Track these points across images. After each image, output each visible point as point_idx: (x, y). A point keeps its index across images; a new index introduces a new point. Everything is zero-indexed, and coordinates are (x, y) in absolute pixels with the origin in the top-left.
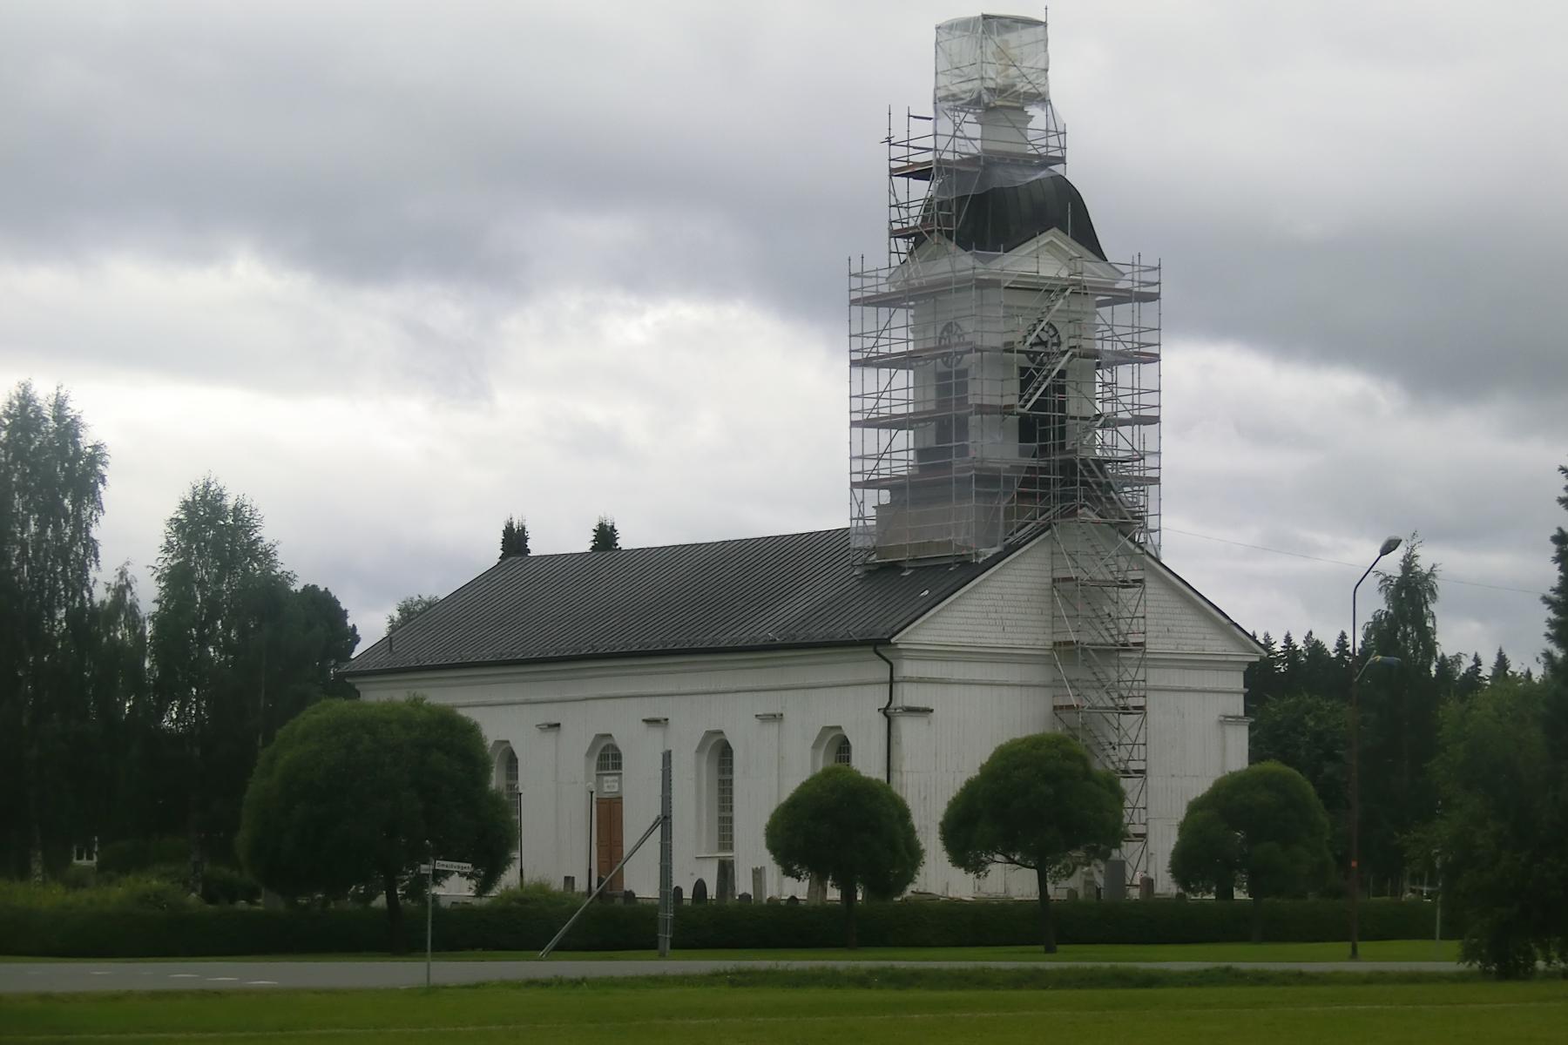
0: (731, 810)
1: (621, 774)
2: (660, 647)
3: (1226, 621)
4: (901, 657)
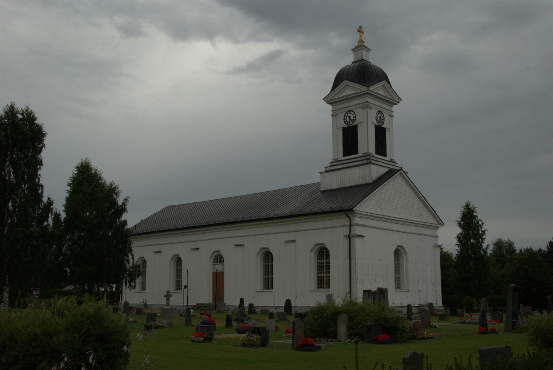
1: (224, 264)
2: (243, 220)
3: (434, 213)
4: (355, 216)
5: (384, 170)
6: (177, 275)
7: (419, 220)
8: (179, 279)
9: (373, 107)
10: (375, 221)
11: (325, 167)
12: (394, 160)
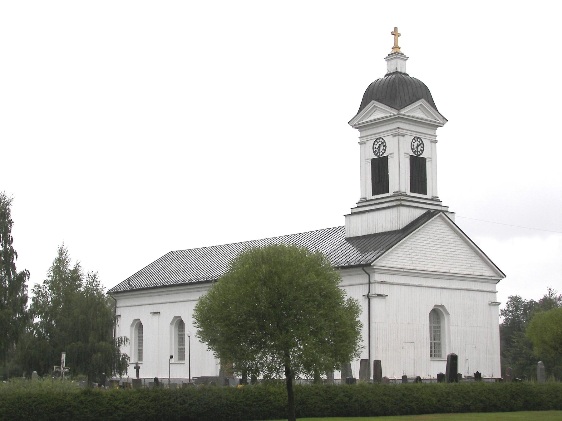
0: (142, 347)
4: (374, 272)
5: (418, 213)
6: (179, 342)
7: (469, 273)
8: (182, 347)
9: (406, 134)
10: (403, 277)
11: (351, 209)
12: (438, 197)
